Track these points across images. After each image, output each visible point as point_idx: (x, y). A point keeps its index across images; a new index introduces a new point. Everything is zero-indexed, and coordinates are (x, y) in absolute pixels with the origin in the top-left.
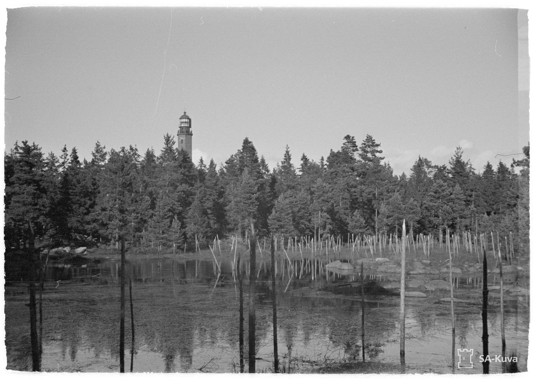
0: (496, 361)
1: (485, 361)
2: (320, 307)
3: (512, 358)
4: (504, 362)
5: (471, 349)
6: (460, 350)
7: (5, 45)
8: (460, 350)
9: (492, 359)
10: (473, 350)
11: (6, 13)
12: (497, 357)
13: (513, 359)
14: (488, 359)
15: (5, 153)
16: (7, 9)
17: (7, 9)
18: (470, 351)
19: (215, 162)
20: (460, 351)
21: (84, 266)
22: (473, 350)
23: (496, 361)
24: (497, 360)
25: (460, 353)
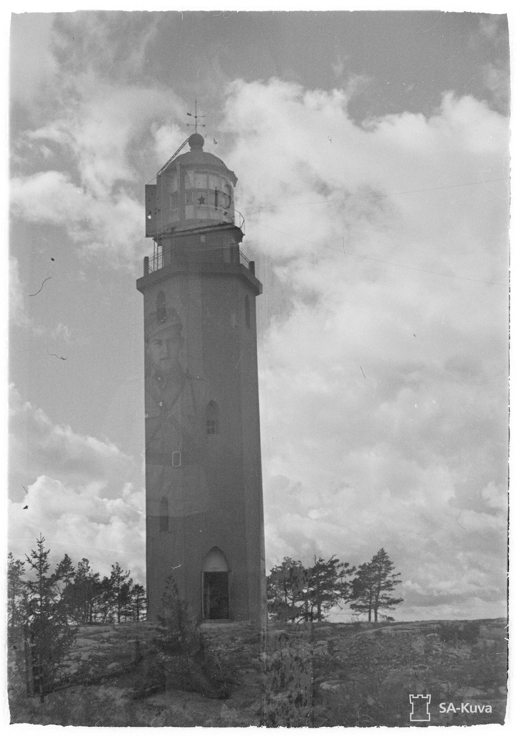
0: (462, 712)
1: (448, 712)
2: (22, 615)
3: (484, 706)
4: (473, 712)
5: (427, 695)
6: (413, 695)
7: (29, 12)
8: (413, 695)
9: (457, 709)
10: (430, 695)
11: (11, 15)
12: (464, 705)
13: (485, 708)
14: (451, 708)
15: (10, 555)
16: (12, 13)
17: (12, 13)
18: (427, 697)
19: (72, 564)
20: (413, 697)
21: (388, 678)
22: (430, 695)
23: (462, 712)
24: (464, 710)
25: (413, 700)
